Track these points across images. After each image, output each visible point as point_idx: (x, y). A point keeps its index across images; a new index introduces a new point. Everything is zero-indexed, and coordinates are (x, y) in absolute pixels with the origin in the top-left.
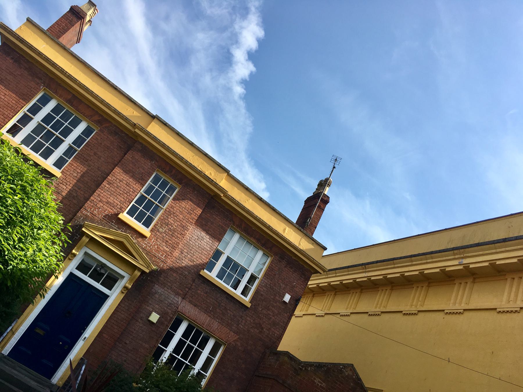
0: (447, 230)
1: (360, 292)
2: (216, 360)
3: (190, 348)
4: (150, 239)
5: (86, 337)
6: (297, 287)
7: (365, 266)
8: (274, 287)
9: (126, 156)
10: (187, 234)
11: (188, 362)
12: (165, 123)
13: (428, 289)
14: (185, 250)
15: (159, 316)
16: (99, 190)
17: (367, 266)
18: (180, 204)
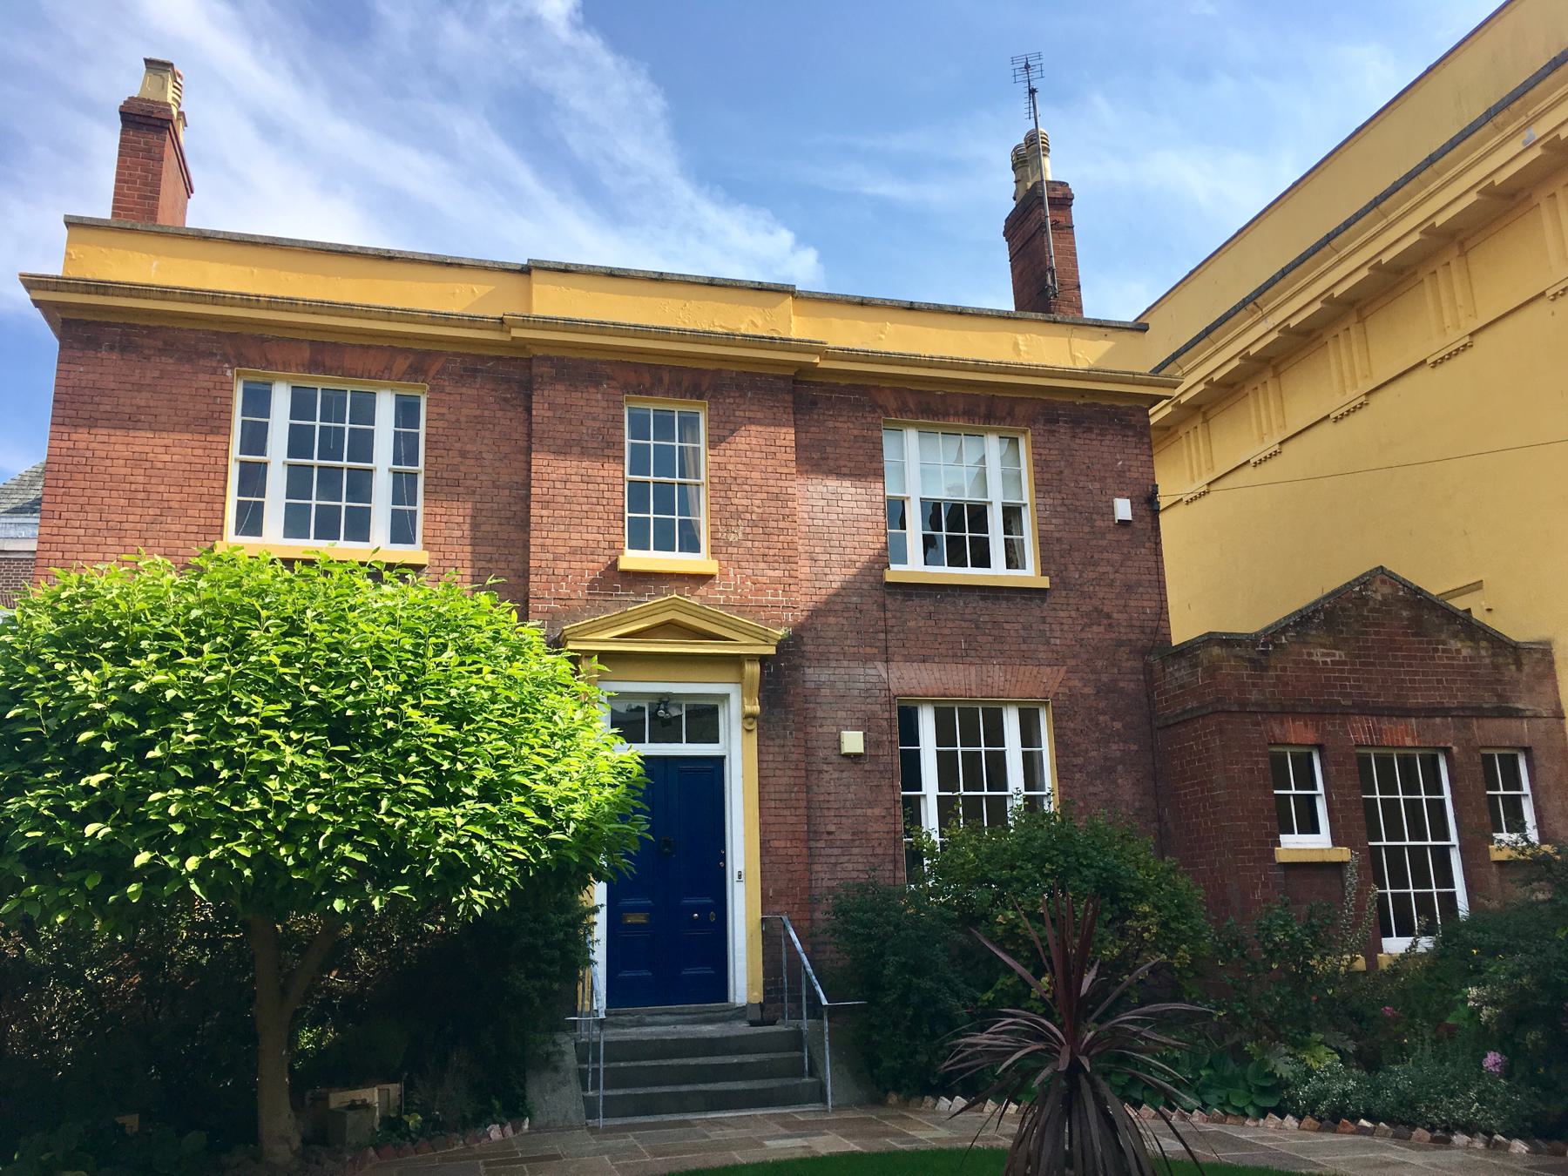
0: (1435, 70)
1: (1273, 377)
2: (1046, 748)
4: (724, 574)
7: (1255, 304)
8: (1078, 503)
9: (534, 413)
10: (799, 509)
11: (1296, 789)
12: (563, 268)
13: (1467, 263)
15: (862, 733)
16: (533, 534)
17: (1259, 301)
18: (734, 446)
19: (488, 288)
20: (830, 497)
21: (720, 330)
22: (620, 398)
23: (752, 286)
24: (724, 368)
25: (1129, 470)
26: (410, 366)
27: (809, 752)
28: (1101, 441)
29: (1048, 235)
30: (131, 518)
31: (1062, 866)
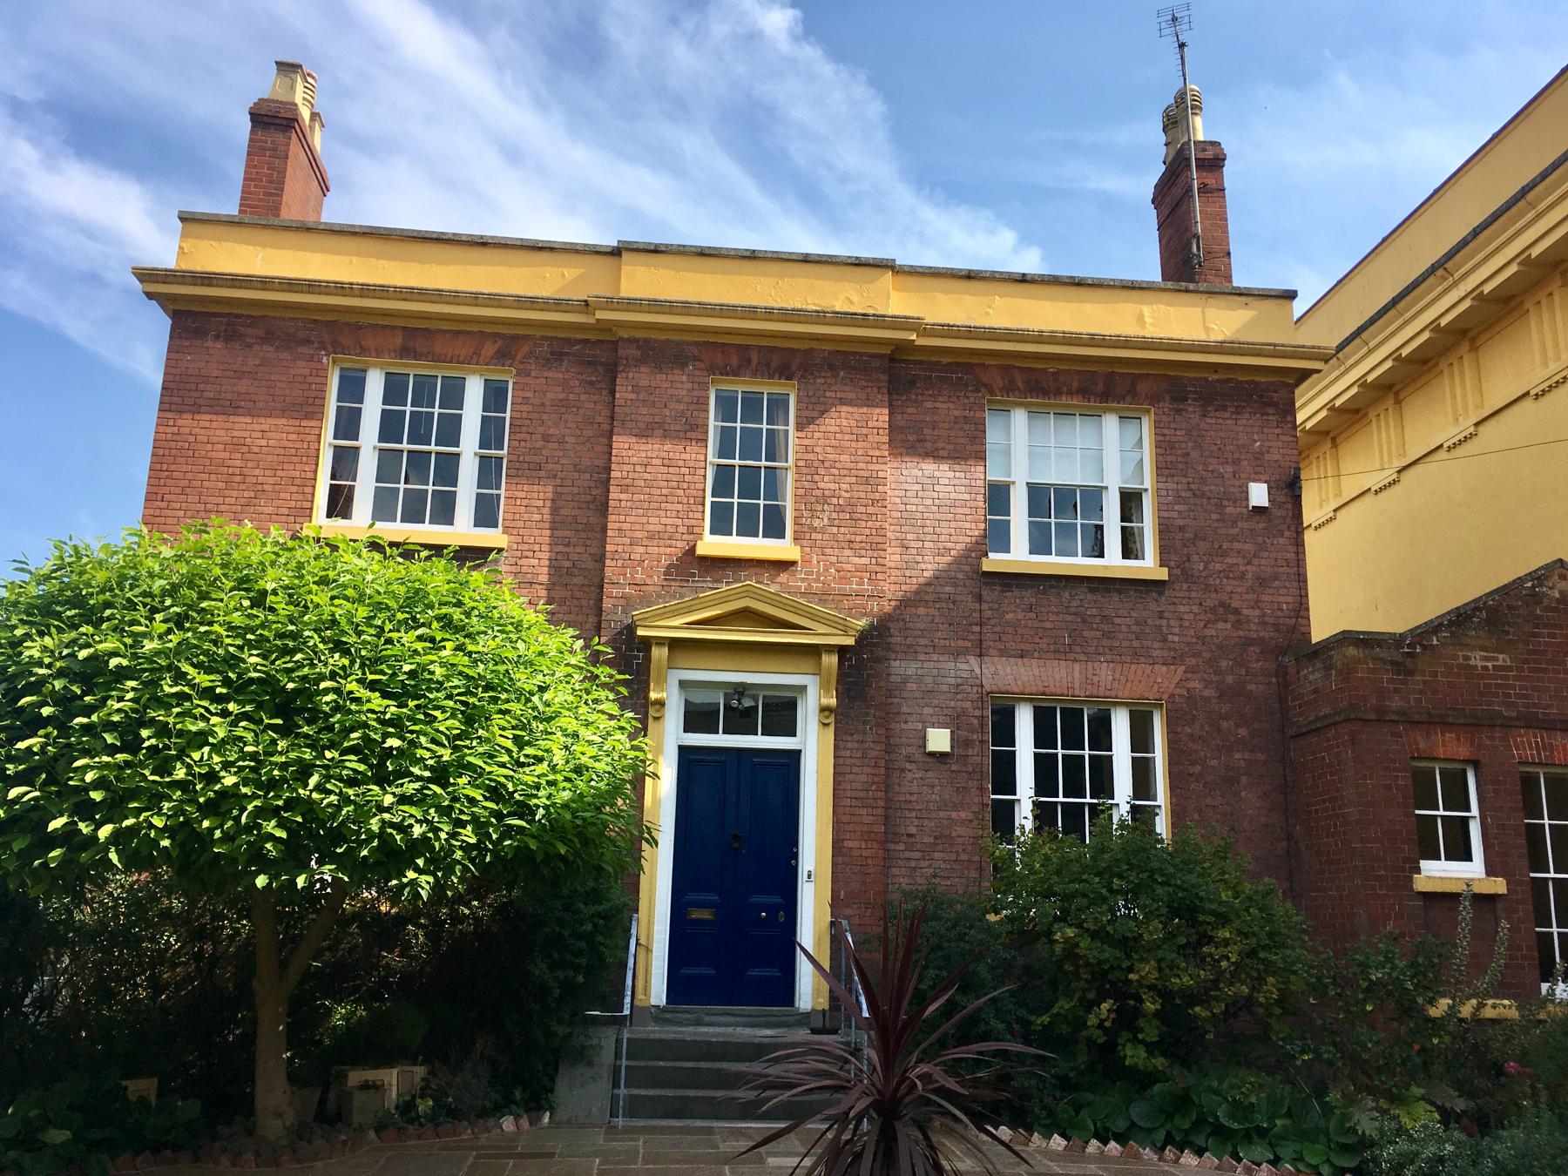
2: (1159, 755)
3: (1073, 764)
7: (1445, 269)
8: (1206, 488)
9: (617, 395)
11: (1444, 810)
12: (653, 248)
14: (909, 536)
16: (611, 518)
17: (1449, 265)
18: (823, 428)
19: (579, 271)
20: (926, 480)
22: (706, 380)
24: (816, 347)
25: (1268, 452)
26: (498, 351)
27: (889, 748)
28: (1236, 420)
29: (1194, 201)
30: (227, 500)
31: (1133, 882)
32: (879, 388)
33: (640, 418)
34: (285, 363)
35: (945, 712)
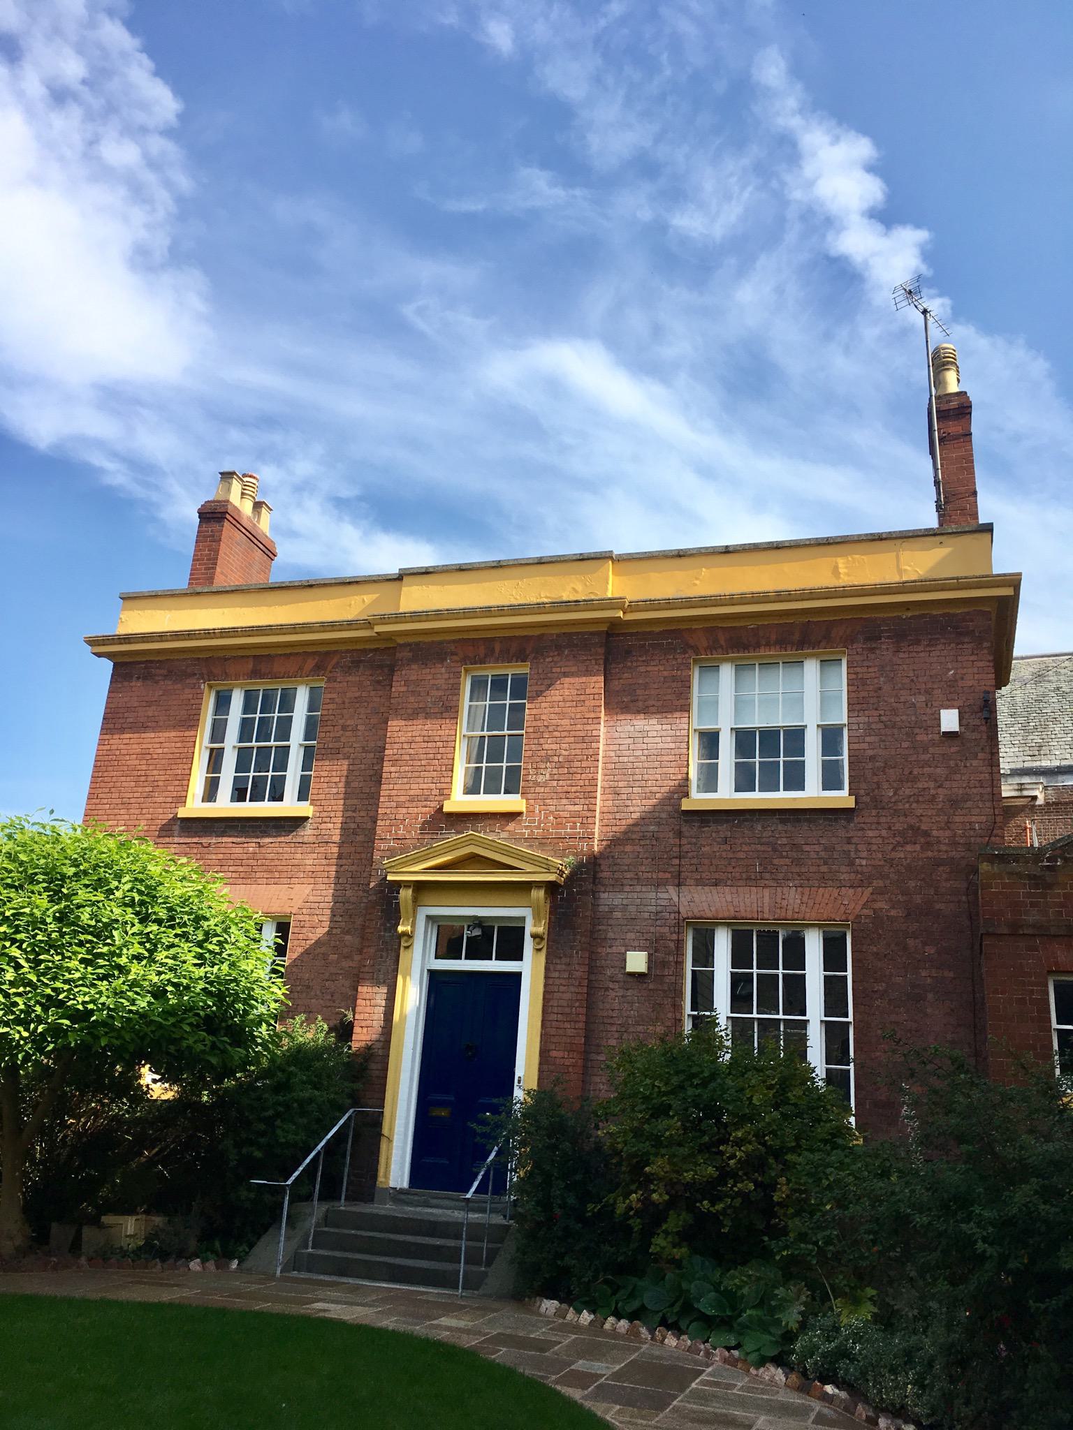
3: (768, 983)
5: (520, 1077)
6: (965, 674)
8: (898, 719)
14: (621, 784)
16: (383, 787)
18: (549, 699)
20: (637, 735)
21: (546, 600)
23: (574, 558)
25: (962, 679)
30: (136, 795)
32: (596, 660)
33: (409, 706)
34: (177, 692)
35: (646, 936)
